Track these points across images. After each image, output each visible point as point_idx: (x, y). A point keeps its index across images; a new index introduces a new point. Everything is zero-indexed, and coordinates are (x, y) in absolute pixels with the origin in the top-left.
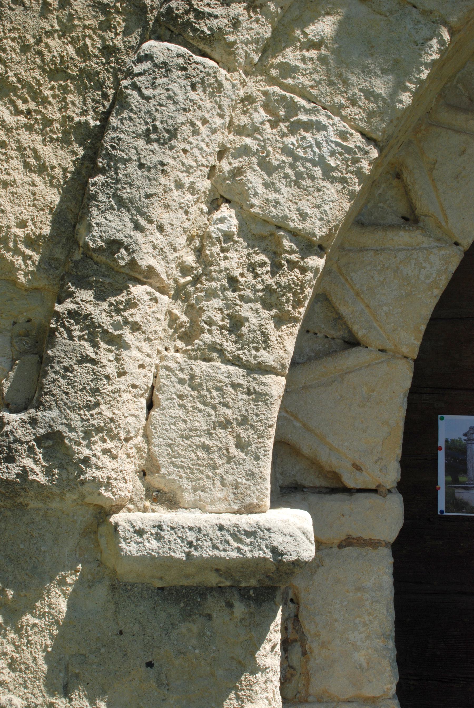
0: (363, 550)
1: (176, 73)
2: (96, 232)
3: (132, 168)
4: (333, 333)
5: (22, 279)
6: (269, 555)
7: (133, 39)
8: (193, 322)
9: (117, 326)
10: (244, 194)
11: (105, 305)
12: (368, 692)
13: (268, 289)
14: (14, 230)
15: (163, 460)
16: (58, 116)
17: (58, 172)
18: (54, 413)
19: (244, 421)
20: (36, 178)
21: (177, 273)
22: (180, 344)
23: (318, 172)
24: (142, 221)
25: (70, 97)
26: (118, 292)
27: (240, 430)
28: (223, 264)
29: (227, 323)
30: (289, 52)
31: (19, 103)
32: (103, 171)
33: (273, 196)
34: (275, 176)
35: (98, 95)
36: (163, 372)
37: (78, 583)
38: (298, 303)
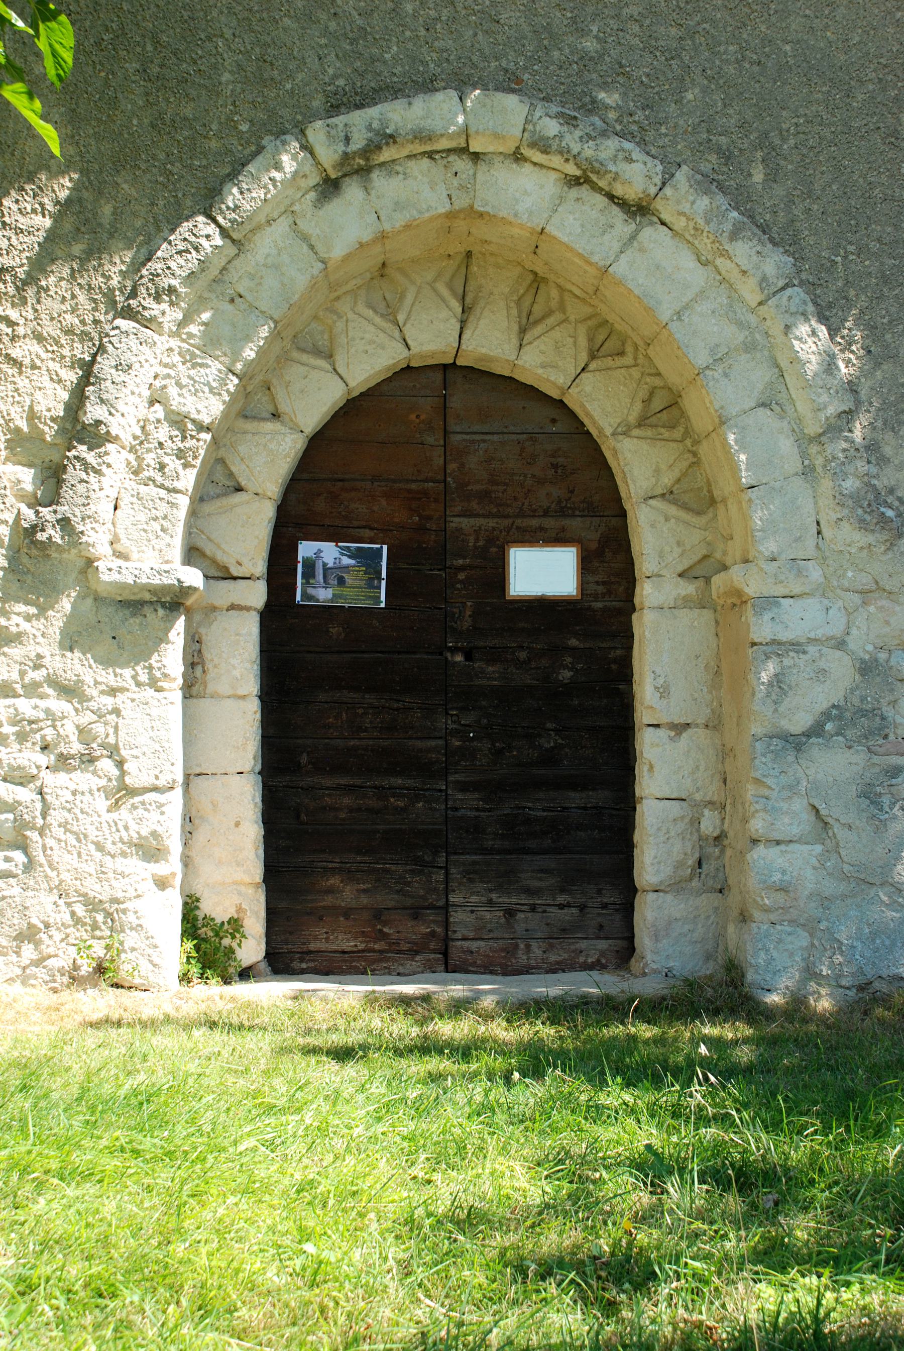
0: (241, 613)
1: (132, 336)
2: (89, 415)
3: (108, 383)
4: (228, 483)
5: (49, 439)
6: (176, 582)
7: (110, 317)
8: (139, 465)
9: (99, 464)
10: (167, 399)
11: (93, 453)
12: (241, 692)
13: (179, 449)
14: (45, 413)
15: (122, 536)
16: (69, 354)
17: (68, 383)
18: (66, 508)
19: (165, 517)
20: (56, 385)
21: (131, 439)
22: (133, 477)
23: (206, 389)
24: (113, 411)
25: (75, 345)
26: (100, 446)
27: (162, 522)
28: (156, 435)
29: (157, 466)
30: (191, 326)
31: (48, 347)
32: (93, 384)
33: (182, 400)
34: (184, 391)
35: (90, 344)
36: (123, 491)
37: (78, 596)
38: (195, 457)
